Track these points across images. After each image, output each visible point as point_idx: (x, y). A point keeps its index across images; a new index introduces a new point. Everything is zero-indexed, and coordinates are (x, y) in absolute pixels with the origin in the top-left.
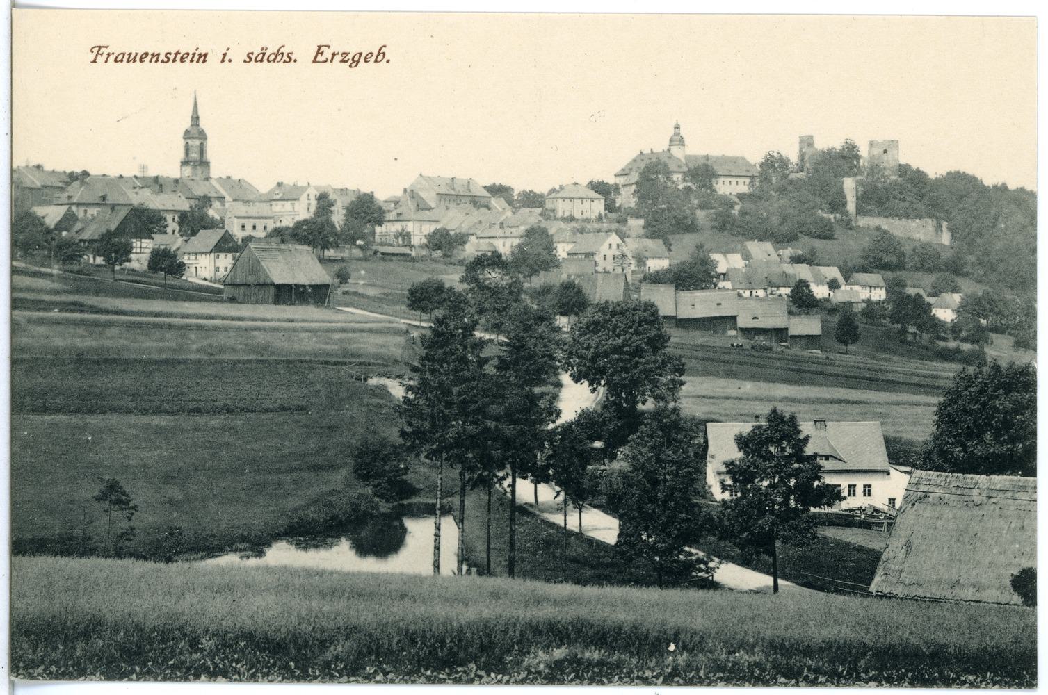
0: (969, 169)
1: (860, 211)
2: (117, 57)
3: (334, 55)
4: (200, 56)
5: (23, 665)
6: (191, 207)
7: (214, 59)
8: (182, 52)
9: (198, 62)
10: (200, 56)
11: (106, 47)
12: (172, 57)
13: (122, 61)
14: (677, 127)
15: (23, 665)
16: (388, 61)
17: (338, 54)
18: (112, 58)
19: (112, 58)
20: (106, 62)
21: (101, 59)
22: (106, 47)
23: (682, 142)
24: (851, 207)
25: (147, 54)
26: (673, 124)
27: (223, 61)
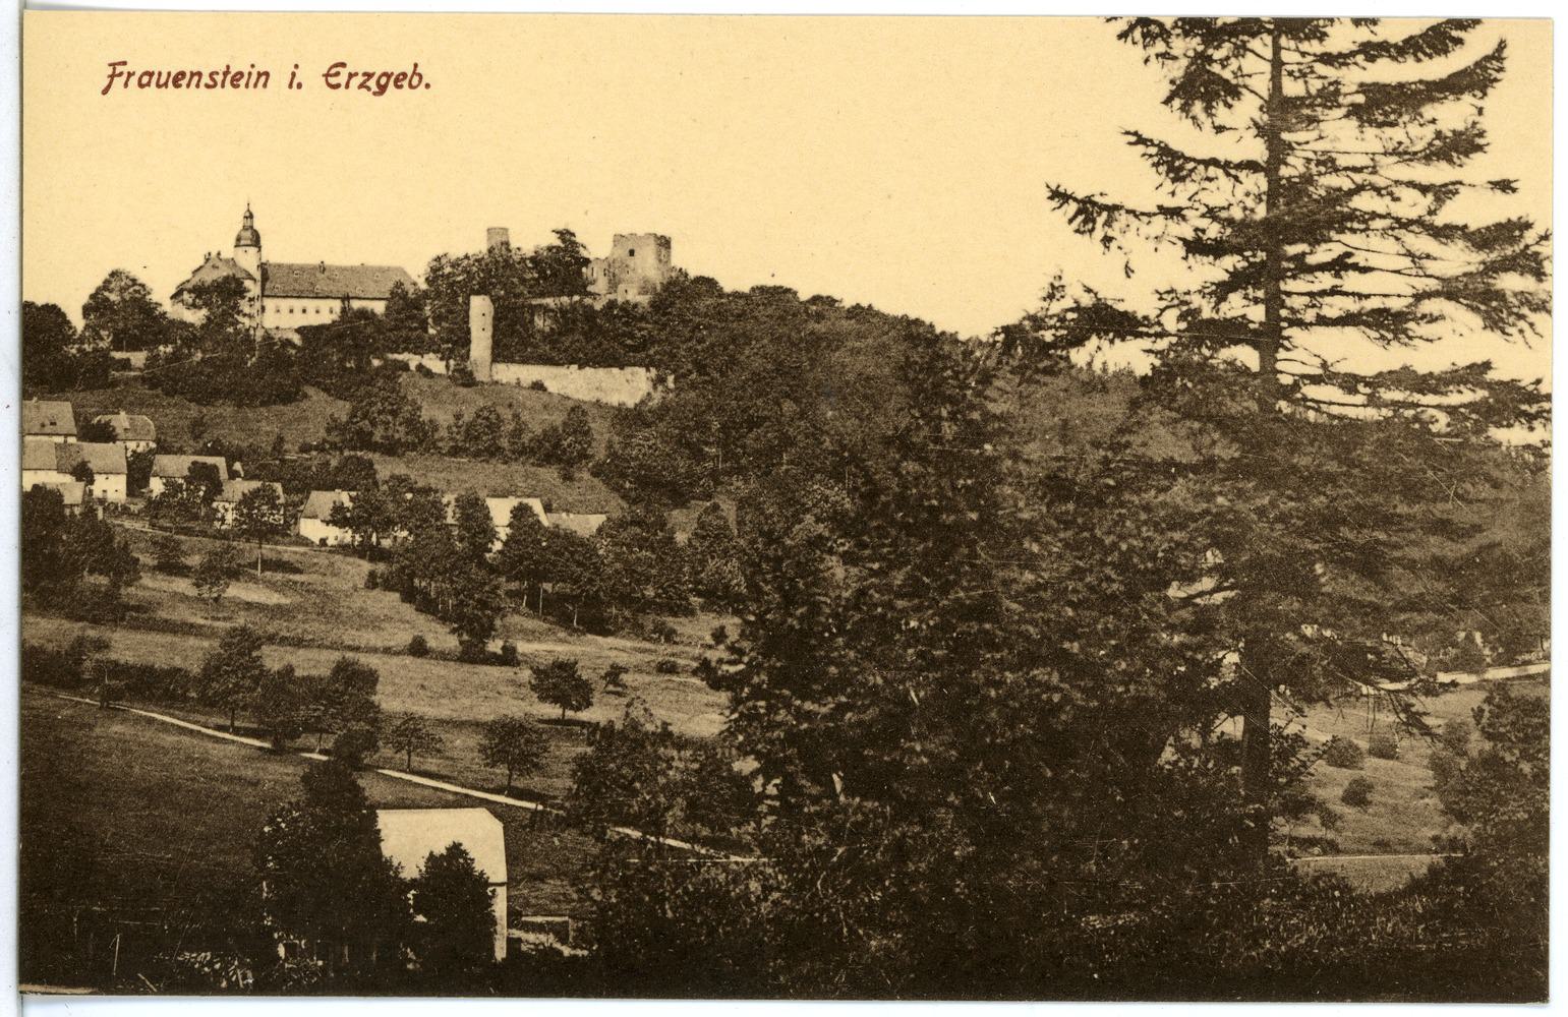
0: (717, 278)
1: (501, 352)
2: (140, 79)
3: (351, 76)
4: (260, 75)
5: (45, 963)
6: (1154, 368)
7: (279, 80)
8: (233, 71)
9: (255, 85)
10: (260, 75)
11: (125, 63)
12: (219, 78)
13: (148, 84)
14: (1059, 196)
15: (45, 963)
16: (428, 86)
17: (356, 74)
18: (134, 81)
19: (134, 81)
20: (105, 92)
21: (119, 82)
22: (125, 63)
23: (256, 241)
25: (183, 74)
26: (243, 211)
27: (290, 86)
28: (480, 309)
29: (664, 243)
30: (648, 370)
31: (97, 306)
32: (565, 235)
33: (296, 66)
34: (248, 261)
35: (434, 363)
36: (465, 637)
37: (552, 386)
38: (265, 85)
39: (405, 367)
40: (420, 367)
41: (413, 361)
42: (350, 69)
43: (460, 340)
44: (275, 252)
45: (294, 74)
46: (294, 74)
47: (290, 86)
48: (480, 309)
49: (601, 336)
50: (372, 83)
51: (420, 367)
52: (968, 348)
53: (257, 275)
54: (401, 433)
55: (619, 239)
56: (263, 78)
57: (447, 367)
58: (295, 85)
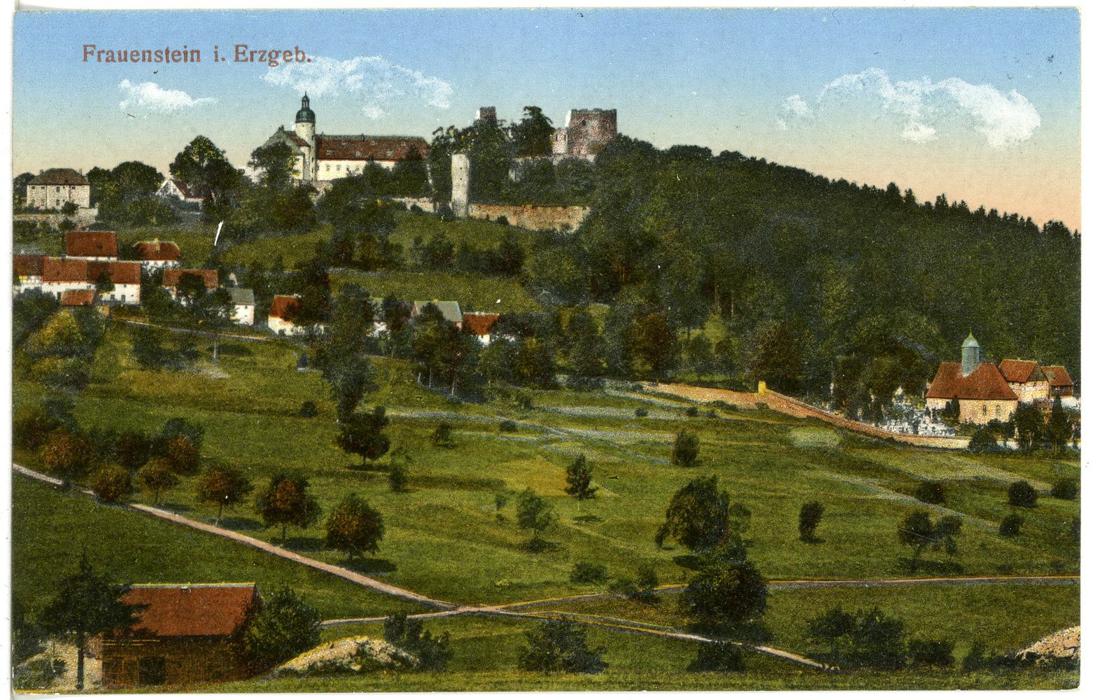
1: (475, 194)
7: (207, 56)
24: (459, 193)
27: (216, 60)
28: (459, 163)
29: (609, 118)
30: (584, 209)
31: (182, 165)
32: (535, 111)
33: (216, 47)
34: (303, 131)
35: (426, 205)
36: (221, 313)
37: (513, 221)
38: (198, 60)
39: (402, 207)
40: (414, 208)
41: (409, 202)
42: (251, 49)
43: (445, 188)
44: (328, 126)
45: (216, 52)
46: (216, 52)
47: (216, 60)
48: (459, 163)
49: (546, 185)
50: (266, 56)
51: (414, 208)
52: (235, 170)
53: (312, 143)
54: (375, 253)
55: (576, 114)
56: (195, 54)
57: (435, 207)
58: (220, 59)
